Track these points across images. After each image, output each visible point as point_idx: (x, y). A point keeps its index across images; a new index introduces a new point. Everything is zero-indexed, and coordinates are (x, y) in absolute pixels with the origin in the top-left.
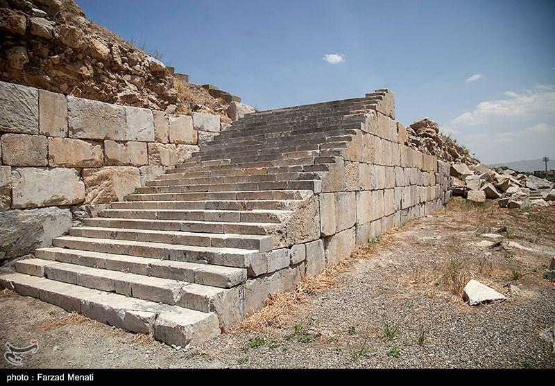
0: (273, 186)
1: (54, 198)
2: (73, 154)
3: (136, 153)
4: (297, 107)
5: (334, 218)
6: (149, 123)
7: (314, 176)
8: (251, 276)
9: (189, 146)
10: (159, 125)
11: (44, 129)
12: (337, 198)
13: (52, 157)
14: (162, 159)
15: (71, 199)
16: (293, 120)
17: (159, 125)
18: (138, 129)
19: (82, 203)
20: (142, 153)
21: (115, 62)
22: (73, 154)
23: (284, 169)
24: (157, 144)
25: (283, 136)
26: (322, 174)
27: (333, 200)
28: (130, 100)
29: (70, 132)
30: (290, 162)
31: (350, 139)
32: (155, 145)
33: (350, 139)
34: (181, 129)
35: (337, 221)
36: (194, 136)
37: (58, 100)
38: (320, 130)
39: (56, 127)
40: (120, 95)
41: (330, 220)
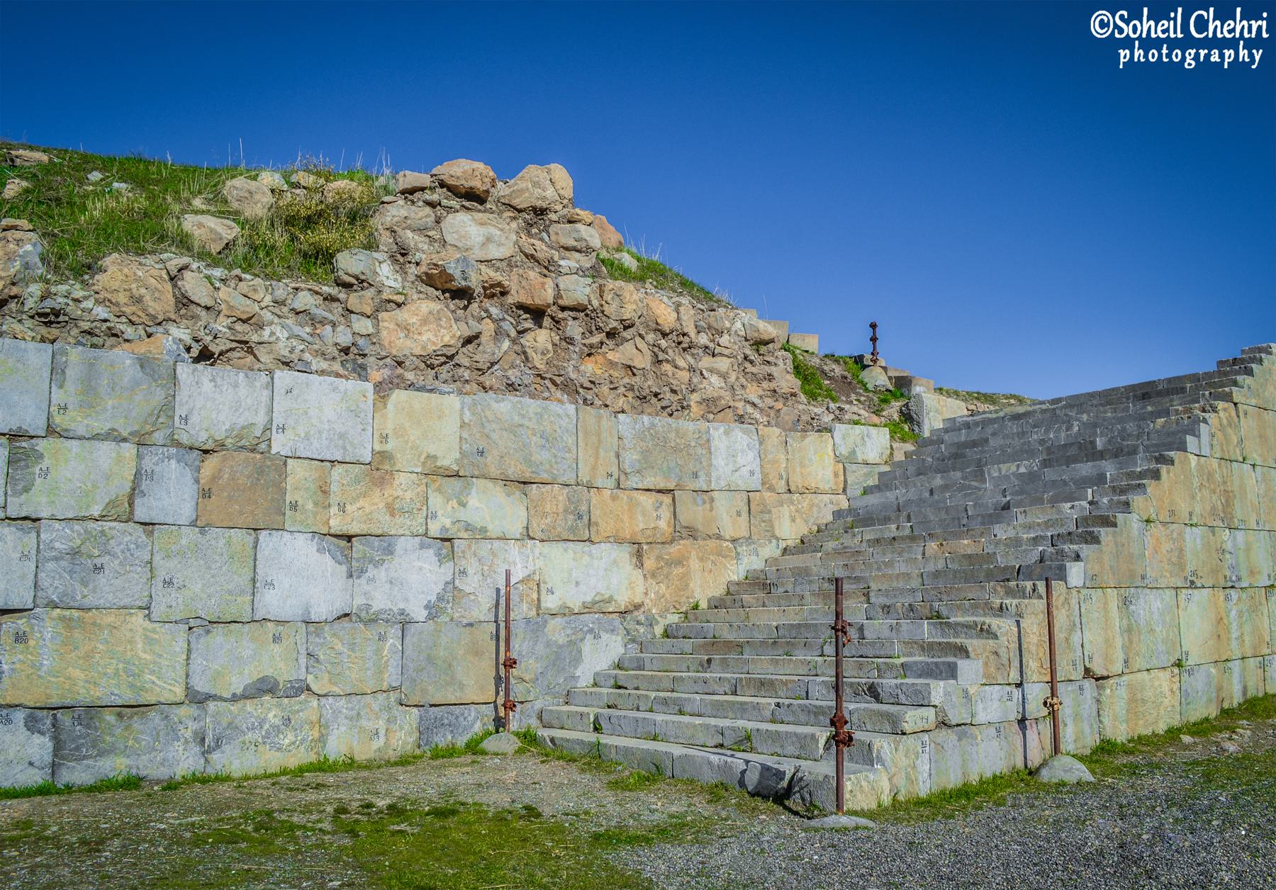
0: (990, 576)
1: (597, 599)
2: (626, 517)
3: (727, 517)
4: (1059, 400)
5: (1119, 642)
6: (751, 455)
7: (963, 651)
8: (943, 724)
9: (826, 498)
10: (770, 457)
11: (584, 478)
12: (1126, 602)
13: (597, 524)
14: (776, 524)
15: (623, 600)
16: (1047, 431)
17: (770, 457)
18: (731, 467)
19: (637, 607)
20: (739, 513)
21: (958, 536)
22: (626, 517)
23: (1016, 542)
24: (767, 495)
25: (1022, 470)
26: (1086, 550)
27: (1114, 604)
28: (713, 408)
29: (623, 478)
30: (1029, 527)
31: (1156, 475)
32: (763, 499)
33: (1156, 475)
34: (810, 460)
35: (1127, 649)
36: (836, 475)
37: (604, 422)
38: (1101, 455)
39: (601, 471)
40: (695, 397)
41: (1108, 642)
